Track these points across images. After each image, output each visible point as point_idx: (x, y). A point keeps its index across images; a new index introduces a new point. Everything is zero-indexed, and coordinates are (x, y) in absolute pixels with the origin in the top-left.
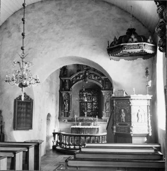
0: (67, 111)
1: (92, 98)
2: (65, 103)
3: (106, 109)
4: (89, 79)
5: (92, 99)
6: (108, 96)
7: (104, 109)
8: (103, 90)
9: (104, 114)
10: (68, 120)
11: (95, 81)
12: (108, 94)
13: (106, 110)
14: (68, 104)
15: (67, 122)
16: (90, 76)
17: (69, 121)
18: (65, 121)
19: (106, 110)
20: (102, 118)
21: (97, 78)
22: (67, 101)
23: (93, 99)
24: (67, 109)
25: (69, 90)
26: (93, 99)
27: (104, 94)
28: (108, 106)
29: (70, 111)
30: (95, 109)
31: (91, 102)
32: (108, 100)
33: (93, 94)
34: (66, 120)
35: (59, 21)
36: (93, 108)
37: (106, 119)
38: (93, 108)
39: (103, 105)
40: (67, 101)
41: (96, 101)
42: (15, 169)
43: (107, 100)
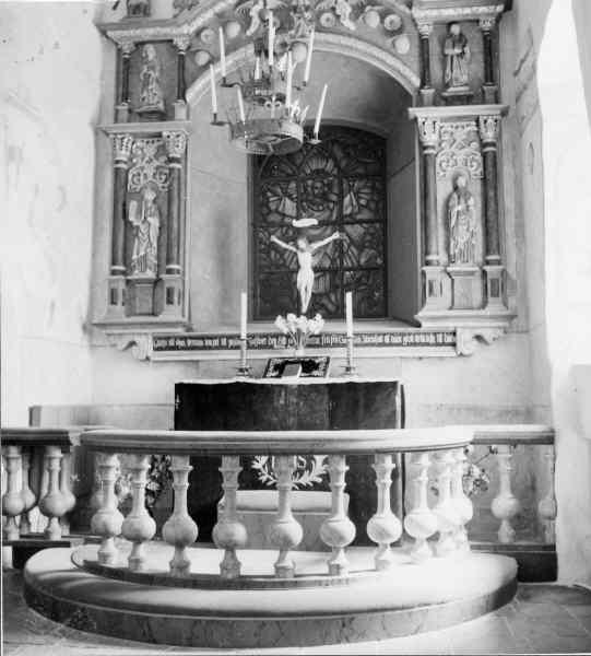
0: (150, 274)
1: (336, 190)
2: (139, 212)
3: (447, 248)
4: (319, 29)
5: (334, 198)
6: (461, 156)
7: (433, 249)
8: (420, 104)
9: (436, 288)
10: (156, 339)
11: (361, 46)
12: (460, 135)
13: (451, 260)
14: (154, 222)
15: (150, 352)
16: (322, 12)
17: (165, 344)
18: (132, 344)
19: (451, 260)
20: (420, 316)
21: (373, 19)
22: (150, 196)
23: (341, 196)
24: (153, 260)
25: (163, 116)
26: (347, 200)
27: (430, 138)
28: (462, 228)
29: (169, 271)
30: (360, 268)
31: (334, 223)
32: (462, 182)
33: (343, 164)
34: (146, 344)
35: (204, 342)
36: (347, 263)
37: (450, 325)
38: (347, 263)
39: (425, 219)
40: (150, 196)
41: (365, 215)
42: (241, 488)
43: (455, 180)
